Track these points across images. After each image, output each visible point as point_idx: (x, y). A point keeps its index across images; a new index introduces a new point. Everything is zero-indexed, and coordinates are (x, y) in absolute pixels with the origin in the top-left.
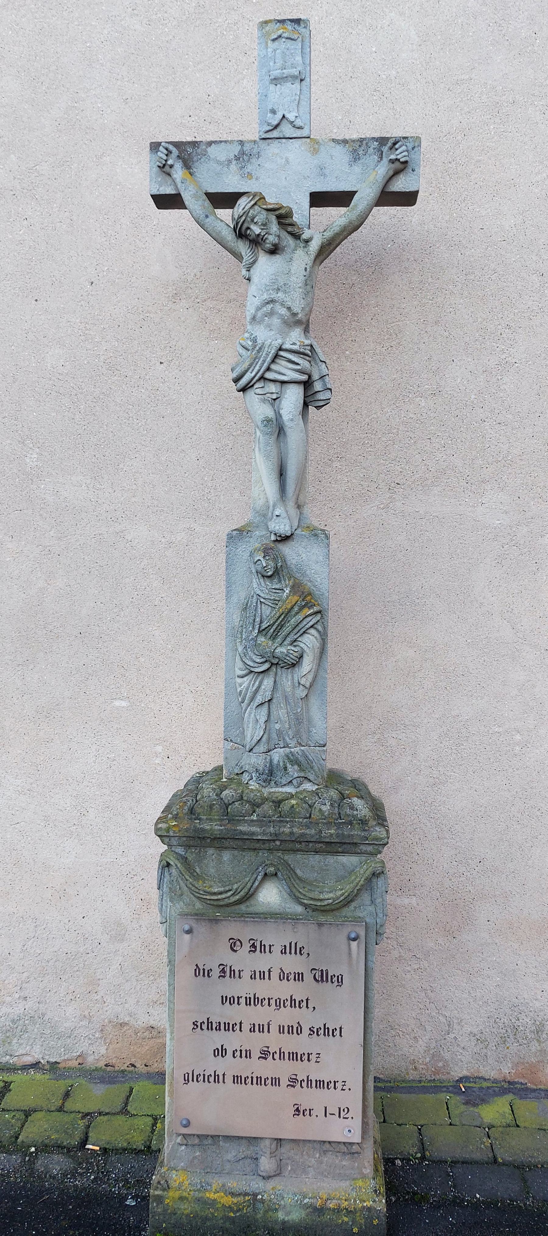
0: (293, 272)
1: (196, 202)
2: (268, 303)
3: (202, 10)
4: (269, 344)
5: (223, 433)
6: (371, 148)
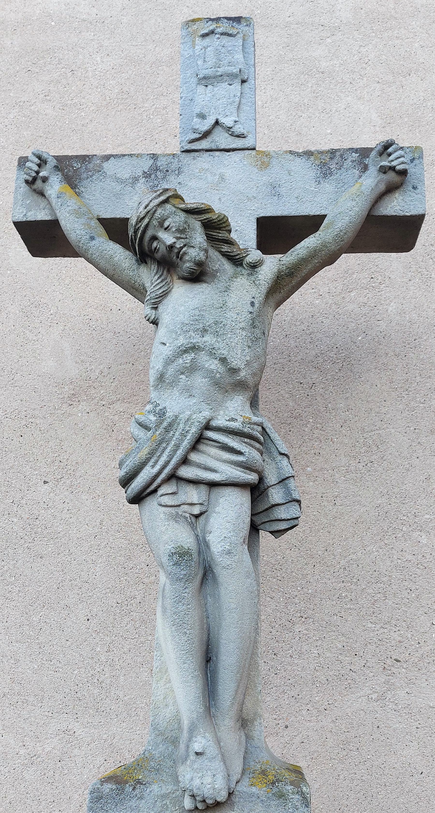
0: (230, 304)
1: (76, 220)
2: (186, 351)
3: (125, 96)
4: (187, 417)
5: (129, 579)
6: (349, 160)
